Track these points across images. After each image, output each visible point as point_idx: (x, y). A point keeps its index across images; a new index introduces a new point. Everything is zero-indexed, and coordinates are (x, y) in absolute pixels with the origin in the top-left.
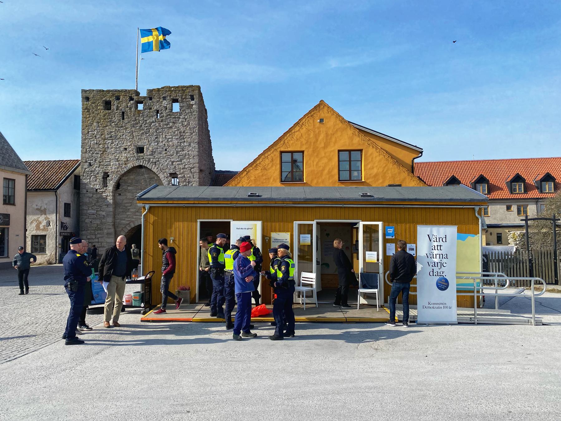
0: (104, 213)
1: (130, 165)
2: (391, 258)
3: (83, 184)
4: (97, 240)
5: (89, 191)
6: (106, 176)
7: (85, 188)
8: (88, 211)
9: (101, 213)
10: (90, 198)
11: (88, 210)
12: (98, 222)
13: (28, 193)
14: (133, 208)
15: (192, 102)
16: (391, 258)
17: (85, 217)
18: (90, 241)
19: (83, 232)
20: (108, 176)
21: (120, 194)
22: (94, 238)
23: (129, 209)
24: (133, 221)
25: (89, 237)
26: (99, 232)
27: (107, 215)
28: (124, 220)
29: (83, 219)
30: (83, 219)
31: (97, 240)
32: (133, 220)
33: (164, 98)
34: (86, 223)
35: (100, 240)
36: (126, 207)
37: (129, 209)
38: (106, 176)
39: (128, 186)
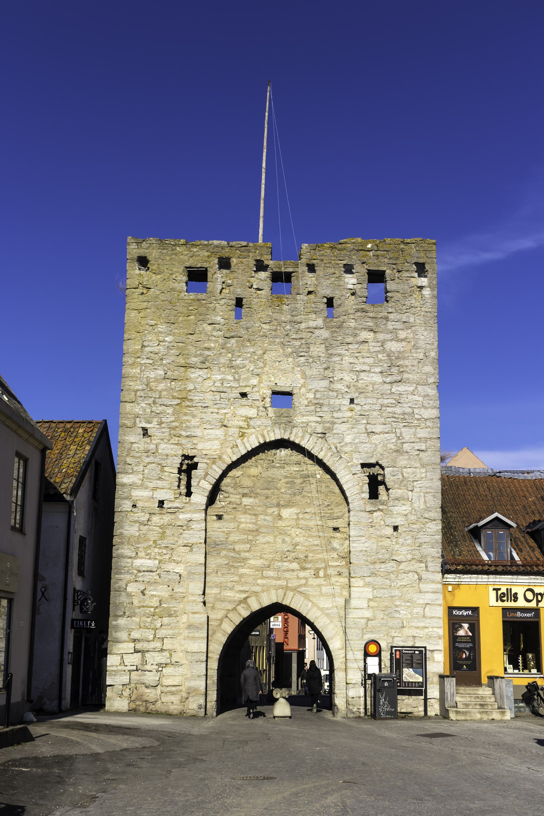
0: (180, 569)
1: (253, 442)
2: (466, 258)
3: (123, 485)
4: (158, 645)
5: (140, 504)
6: (188, 466)
7: (128, 498)
8: (138, 562)
9: (170, 567)
10: (142, 524)
11: (137, 556)
12: (162, 591)
13: (46, 507)
14: (255, 558)
15: (424, 281)
16: (466, 258)
17: (128, 577)
18: (139, 646)
19: (122, 621)
20: (195, 466)
21: (220, 517)
22: (151, 637)
23: (245, 559)
24: (256, 593)
25: (135, 635)
26: (166, 620)
27: (190, 573)
28: (232, 589)
29: (122, 584)
30: (122, 584)
31: (158, 645)
32: (257, 589)
33: (349, 269)
34: (129, 595)
35: (168, 644)
36: (239, 553)
37: (245, 559)
38: (188, 466)
39: (244, 495)
